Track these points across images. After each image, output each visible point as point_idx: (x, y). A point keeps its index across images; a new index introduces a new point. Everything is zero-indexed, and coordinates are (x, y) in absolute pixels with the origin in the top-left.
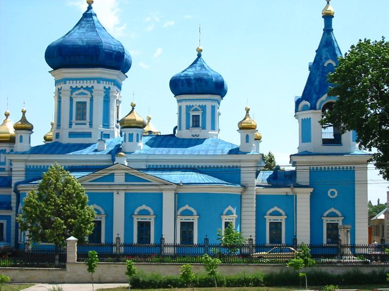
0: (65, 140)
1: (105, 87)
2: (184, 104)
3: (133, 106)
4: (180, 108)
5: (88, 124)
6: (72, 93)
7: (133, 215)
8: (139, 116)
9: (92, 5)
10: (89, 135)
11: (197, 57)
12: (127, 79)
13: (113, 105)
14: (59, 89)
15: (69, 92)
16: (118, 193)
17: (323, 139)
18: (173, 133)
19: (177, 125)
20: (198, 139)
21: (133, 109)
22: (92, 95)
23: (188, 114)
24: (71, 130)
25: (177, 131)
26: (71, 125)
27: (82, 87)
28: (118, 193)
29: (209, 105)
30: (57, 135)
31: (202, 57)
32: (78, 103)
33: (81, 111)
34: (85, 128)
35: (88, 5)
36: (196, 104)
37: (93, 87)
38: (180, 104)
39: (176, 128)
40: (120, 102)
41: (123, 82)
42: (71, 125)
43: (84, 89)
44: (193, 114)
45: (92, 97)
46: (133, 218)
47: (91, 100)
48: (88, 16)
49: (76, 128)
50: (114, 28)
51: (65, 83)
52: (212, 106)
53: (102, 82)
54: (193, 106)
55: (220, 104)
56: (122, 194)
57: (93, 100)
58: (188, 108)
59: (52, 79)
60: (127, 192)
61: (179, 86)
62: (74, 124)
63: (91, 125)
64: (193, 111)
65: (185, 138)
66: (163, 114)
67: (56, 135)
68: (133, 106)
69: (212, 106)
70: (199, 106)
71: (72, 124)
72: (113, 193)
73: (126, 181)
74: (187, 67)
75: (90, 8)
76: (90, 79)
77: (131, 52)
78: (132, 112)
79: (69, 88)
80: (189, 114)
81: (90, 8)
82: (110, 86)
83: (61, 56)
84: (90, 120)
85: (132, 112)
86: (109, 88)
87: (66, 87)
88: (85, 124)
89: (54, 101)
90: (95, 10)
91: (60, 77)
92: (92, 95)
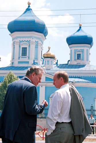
0: (16, 65)
1: (36, 41)
2: (73, 49)
3: (49, 48)
4: (71, 51)
5: (27, 58)
6: (20, 43)
7: (49, 97)
8: (52, 53)
9: (30, 5)
10: (28, 62)
11: (79, 28)
12: (46, 40)
13: (39, 48)
14: (14, 42)
15: (19, 43)
16: (42, 87)
17: (3, 142)
18: (67, 63)
19: (69, 59)
20: (80, 65)
21: (49, 50)
22: (29, 44)
23: (75, 53)
24: (20, 61)
25: (69, 62)
26: (19, 58)
27: (25, 41)
28: (42, 87)
29: (85, 49)
30: (13, 63)
31: (82, 28)
32: (23, 48)
33: (24, 52)
34: (26, 59)
35: (28, 5)
36: (79, 48)
37: (30, 41)
38: (71, 49)
39: (69, 61)
40: (43, 49)
41: (44, 41)
42: (19, 58)
43: (26, 41)
44: (78, 53)
45: (30, 45)
46: (49, 99)
47: (29, 47)
48: (28, 9)
49: (22, 59)
50: (41, 15)
51: (17, 39)
52: (87, 50)
53: (34, 38)
54: (77, 49)
55: (92, 47)
56: (44, 87)
57: (30, 47)
58: (75, 51)
59: (10, 38)
60: (46, 86)
61: (72, 41)
62: (21, 58)
63: (29, 58)
64: (78, 52)
65: (74, 64)
66: (64, 54)
67: (12, 63)
68: (49, 48)
69: (87, 50)
70: (81, 49)
71: (20, 58)
72: (39, 87)
73: (46, 81)
74: (75, 32)
75: (29, 6)
76: (29, 37)
77: (49, 31)
78: (49, 51)
79: (19, 41)
80: (76, 53)
81: (29, 6)
82: (38, 41)
83: (15, 27)
84: (28, 56)
85: (49, 51)
86: (38, 41)
87: (18, 40)
88: (26, 58)
89: (11, 47)
90: (31, 7)
91: (15, 36)
92: (29, 44)
